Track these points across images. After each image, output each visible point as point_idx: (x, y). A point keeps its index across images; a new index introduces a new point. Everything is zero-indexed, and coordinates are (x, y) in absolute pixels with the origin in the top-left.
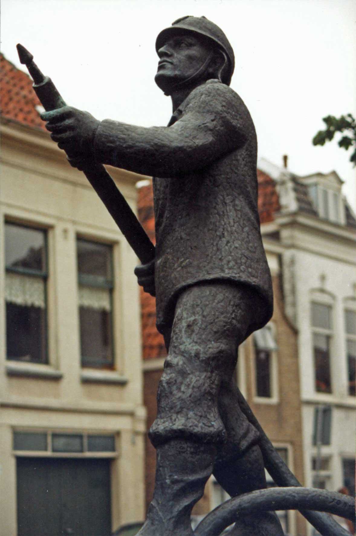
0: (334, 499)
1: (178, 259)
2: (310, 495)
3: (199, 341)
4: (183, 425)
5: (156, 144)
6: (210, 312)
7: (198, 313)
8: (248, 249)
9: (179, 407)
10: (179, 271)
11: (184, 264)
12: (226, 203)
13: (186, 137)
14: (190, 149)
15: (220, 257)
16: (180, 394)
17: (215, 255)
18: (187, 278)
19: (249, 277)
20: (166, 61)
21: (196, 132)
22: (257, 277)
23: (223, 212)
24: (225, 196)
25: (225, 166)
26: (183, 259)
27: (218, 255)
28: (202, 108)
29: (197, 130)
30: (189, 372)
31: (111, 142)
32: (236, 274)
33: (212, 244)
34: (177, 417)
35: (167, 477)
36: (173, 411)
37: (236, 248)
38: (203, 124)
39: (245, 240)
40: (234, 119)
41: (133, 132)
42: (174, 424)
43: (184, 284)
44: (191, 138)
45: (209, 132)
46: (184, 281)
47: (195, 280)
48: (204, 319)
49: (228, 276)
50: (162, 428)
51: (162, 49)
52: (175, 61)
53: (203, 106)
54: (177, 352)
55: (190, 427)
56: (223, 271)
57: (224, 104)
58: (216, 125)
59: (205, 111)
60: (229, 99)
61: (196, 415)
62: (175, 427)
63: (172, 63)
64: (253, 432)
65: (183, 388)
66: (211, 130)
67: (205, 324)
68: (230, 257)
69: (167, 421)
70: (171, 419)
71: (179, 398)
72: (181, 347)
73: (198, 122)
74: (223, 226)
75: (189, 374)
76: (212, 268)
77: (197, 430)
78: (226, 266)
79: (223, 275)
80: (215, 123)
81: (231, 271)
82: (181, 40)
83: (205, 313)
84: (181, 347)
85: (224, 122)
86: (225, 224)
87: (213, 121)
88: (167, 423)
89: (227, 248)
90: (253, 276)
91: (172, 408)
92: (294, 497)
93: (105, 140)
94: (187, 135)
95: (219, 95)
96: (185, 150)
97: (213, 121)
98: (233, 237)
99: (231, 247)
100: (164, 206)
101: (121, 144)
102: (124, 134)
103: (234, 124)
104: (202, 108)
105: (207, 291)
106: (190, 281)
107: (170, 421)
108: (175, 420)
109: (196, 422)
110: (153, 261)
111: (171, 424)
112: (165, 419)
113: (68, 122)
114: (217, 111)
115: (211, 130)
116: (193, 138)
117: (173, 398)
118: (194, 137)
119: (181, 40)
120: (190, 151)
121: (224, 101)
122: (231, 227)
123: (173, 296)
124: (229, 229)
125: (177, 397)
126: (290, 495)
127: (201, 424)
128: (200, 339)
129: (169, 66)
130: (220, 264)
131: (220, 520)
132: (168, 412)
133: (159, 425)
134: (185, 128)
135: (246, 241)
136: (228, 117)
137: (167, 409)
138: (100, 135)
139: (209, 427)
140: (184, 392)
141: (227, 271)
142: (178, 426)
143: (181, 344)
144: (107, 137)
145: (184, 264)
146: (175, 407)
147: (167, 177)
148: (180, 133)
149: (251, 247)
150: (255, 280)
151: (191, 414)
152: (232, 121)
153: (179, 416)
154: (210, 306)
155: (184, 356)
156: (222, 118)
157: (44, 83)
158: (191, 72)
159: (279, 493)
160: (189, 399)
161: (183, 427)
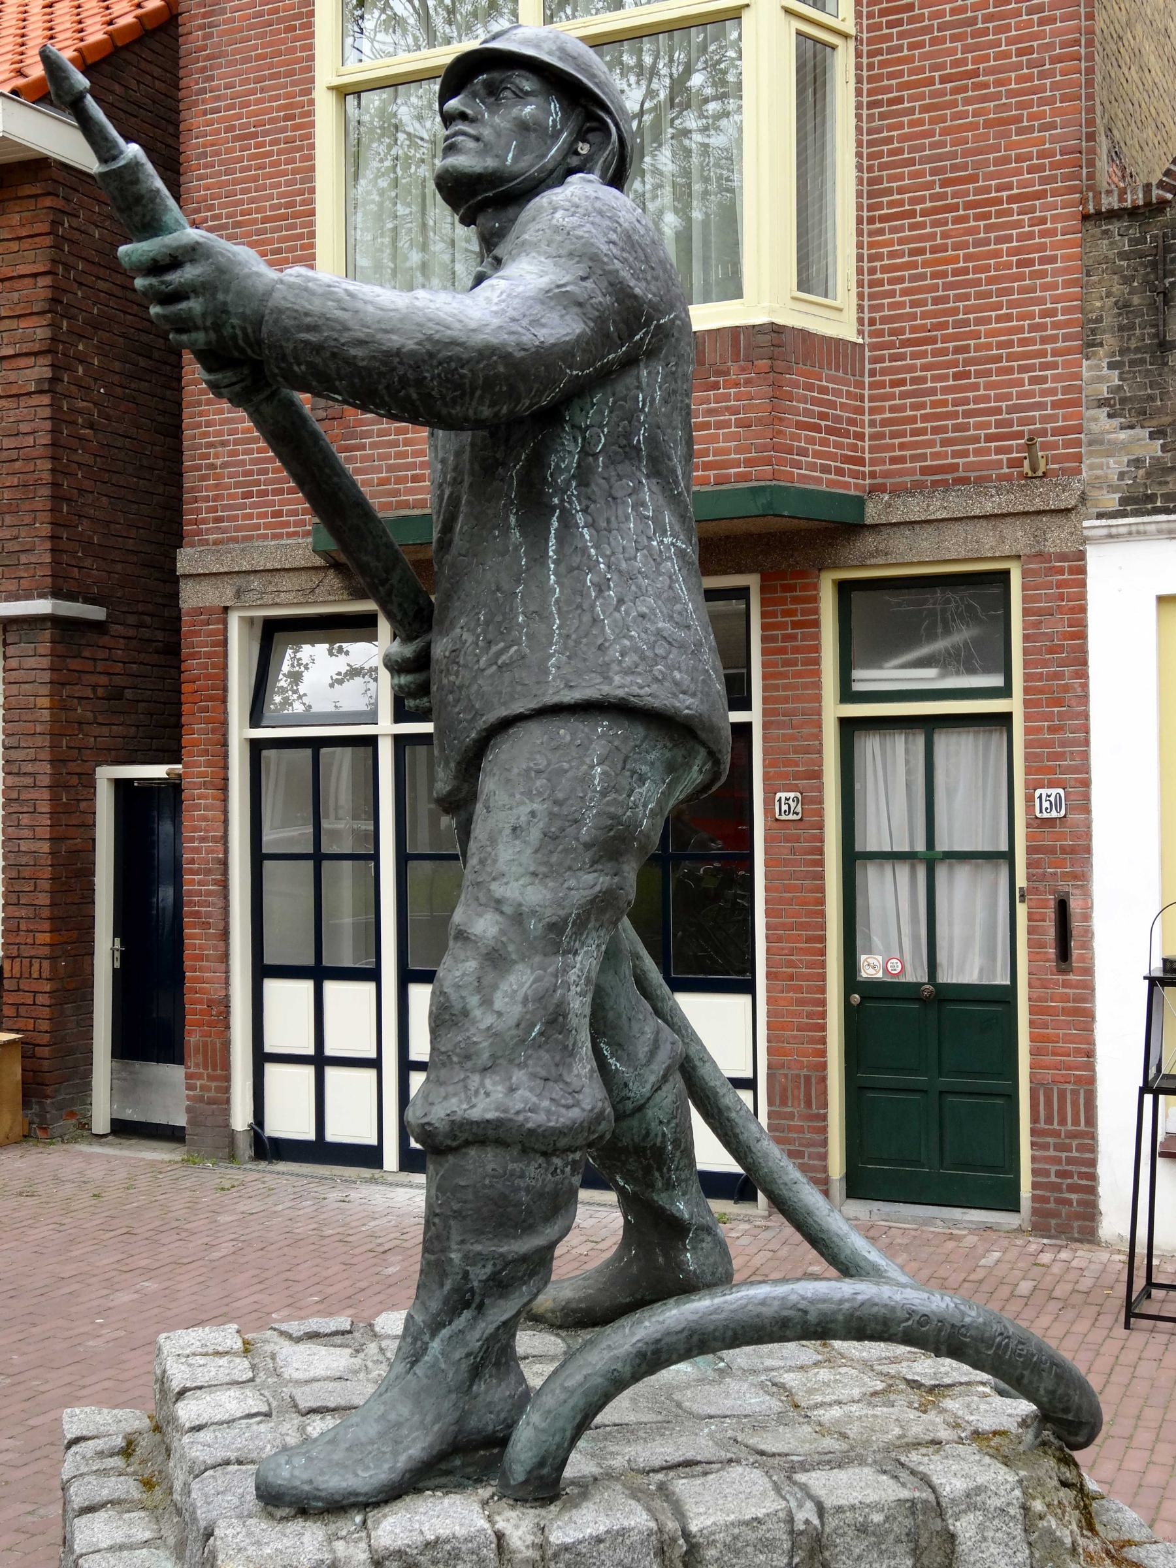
0: (911, 1313)
1: (490, 643)
2: (847, 1306)
3: (543, 869)
4: (497, 1109)
5: (429, 338)
6: (573, 790)
7: (540, 794)
8: (671, 617)
9: (486, 1055)
10: (492, 676)
11: (504, 658)
12: (614, 499)
13: (513, 320)
14: (523, 353)
15: (599, 642)
16: (489, 1020)
17: (586, 636)
18: (513, 699)
19: (675, 695)
20: (464, 134)
21: (539, 307)
22: (694, 695)
23: (608, 521)
24: (613, 480)
25: (598, 414)
26: (502, 645)
27: (596, 636)
28: (554, 245)
29: (543, 303)
30: (514, 957)
31: (311, 328)
32: (641, 687)
33: (579, 606)
34: (482, 1084)
35: (455, 1247)
36: (469, 1064)
37: (643, 616)
38: (558, 286)
39: (665, 595)
40: (638, 279)
41: (365, 302)
42: (473, 1106)
43: (504, 712)
44: (525, 323)
45: (576, 310)
46: (504, 704)
47: (534, 704)
48: (556, 809)
49: (621, 693)
50: (442, 1114)
51: (453, 104)
52: (486, 132)
53: (559, 238)
54: (483, 900)
55: (518, 1113)
56: (608, 679)
57: (614, 237)
58: (593, 290)
59: (563, 252)
60: (626, 225)
61: (534, 1076)
62: (476, 1114)
63: (477, 139)
64: (669, 1046)
65: (498, 1004)
66: (580, 305)
67: (558, 823)
68: (627, 642)
69: (455, 1095)
70: (466, 1088)
71: (489, 1028)
72: (494, 886)
73: (544, 282)
74: (609, 557)
75: (515, 962)
76: (579, 673)
77: (536, 1120)
78: (615, 667)
79: (606, 689)
80: (589, 284)
81: (629, 679)
82: (502, 81)
83: (560, 796)
84: (494, 886)
85: (611, 284)
86: (613, 553)
87: (583, 279)
88: (454, 1100)
89: (617, 615)
90: (684, 693)
91: (468, 1057)
92: (805, 1312)
93: (292, 322)
94: (515, 314)
95: (601, 213)
96: (510, 354)
97: (583, 279)
98: (633, 588)
99: (627, 613)
100: (454, 501)
101: (336, 336)
102: (345, 309)
103: (637, 291)
104: (554, 245)
105: (564, 731)
106: (518, 707)
107: (463, 1095)
108: (477, 1092)
109: (534, 1099)
110: (427, 638)
111: (465, 1106)
112: (451, 1089)
113: (189, 273)
114: (596, 254)
115: (580, 305)
116: (532, 322)
117: (473, 1030)
118: (536, 322)
119: (502, 81)
120: (523, 358)
121: (615, 231)
122: (627, 560)
123: (475, 741)
124: (624, 565)
125: (483, 1026)
126: (794, 1307)
127: (546, 1103)
128: (546, 863)
129: (471, 144)
130: (600, 661)
131: (600, 1380)
132: (457, 1067)
133: (432, 1104)
134: (509, 296)
135: (668, 599)
136: (625, 274)
137: (455, 1059)
138: (280, 311)
139: (568, 1107)
140: (499, 1014)
141: (617, 679)
142: (485, 1110)
143: (494, 879)
144: (298, 315)
145: (504, 658)
146: (477, 1054)
147: (462, 429)
148: (495, 308)
149: (680, 613)
150: (689, 701)
151: (519, 1076)
152: (632, 283)
153: (488, 1082)
154: (569, 775)
155: (502, 912)
156: (606, 273)
157: (122, 163)
158: (527, 84)
159: (763, 1303)
160: (514, 1032)
161: (497, 1114)
